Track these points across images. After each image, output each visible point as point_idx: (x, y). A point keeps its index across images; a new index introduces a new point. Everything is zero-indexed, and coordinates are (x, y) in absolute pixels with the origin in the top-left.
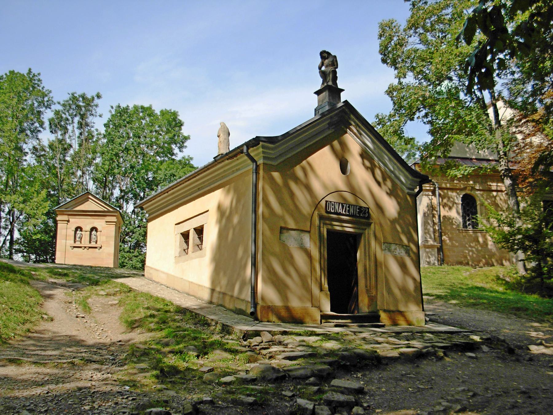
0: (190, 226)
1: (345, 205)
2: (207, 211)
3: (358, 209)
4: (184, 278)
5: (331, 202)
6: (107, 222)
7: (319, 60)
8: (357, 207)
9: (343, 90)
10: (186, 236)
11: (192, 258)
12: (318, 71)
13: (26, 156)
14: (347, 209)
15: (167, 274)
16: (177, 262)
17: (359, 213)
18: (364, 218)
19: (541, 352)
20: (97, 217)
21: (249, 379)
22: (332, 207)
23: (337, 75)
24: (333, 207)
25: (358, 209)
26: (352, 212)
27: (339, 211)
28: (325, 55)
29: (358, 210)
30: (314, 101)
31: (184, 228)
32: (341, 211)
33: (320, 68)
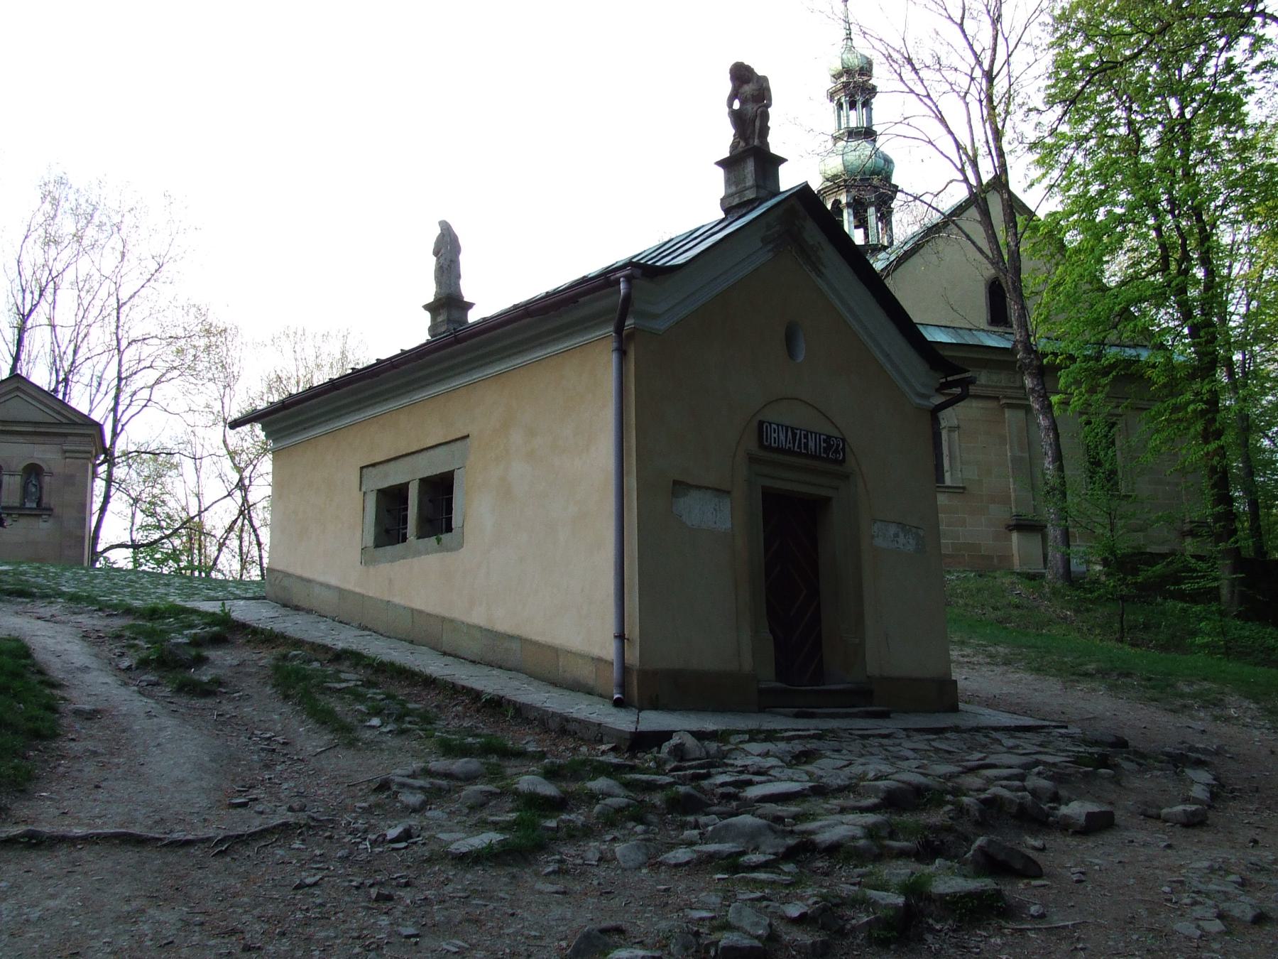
0: (409, 474)
1: (798, 432)
2: (468, 436)
3: (825, 441)
4: (397, 600)
5: (770, 424)
6: (65, 452)
7: (727, 87)
8: (822, 437)
9: (782, 160)
10: (392, 500)
11: (418, 553)
12: (727, 110)
13: (840, 202)
14: (803, 440)
15: (340, 590)
16: (367, 559)
17: (826, 450)
18: (836, 461)
19: (609, 780)
20: (21, 439)
21: (823, 846)
22: (773, 435)
23: (769, 124)
24: (776, 435)
25: (825, 441)
26: (813, 450)
27: (788, 445)
28: (741, 75)
29: (823, 445)
30: (716, 185)
31: (393, 476)
32: (791, 445)
33: (730, 104)
